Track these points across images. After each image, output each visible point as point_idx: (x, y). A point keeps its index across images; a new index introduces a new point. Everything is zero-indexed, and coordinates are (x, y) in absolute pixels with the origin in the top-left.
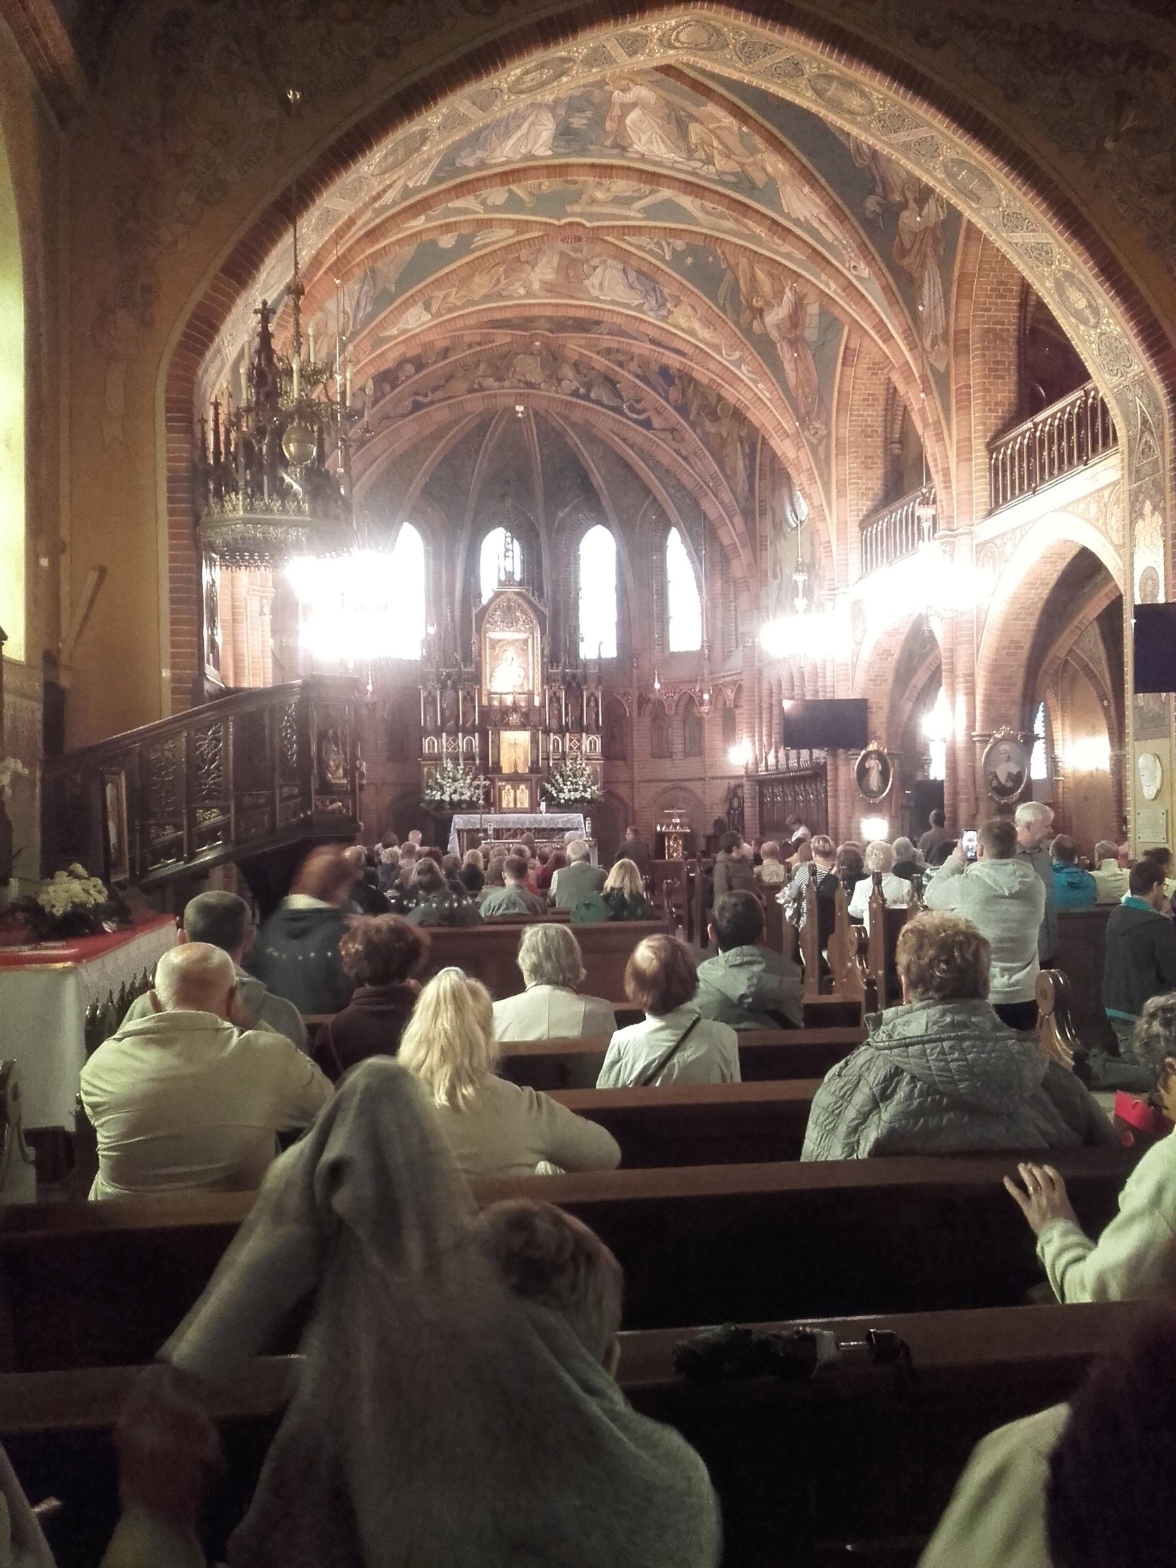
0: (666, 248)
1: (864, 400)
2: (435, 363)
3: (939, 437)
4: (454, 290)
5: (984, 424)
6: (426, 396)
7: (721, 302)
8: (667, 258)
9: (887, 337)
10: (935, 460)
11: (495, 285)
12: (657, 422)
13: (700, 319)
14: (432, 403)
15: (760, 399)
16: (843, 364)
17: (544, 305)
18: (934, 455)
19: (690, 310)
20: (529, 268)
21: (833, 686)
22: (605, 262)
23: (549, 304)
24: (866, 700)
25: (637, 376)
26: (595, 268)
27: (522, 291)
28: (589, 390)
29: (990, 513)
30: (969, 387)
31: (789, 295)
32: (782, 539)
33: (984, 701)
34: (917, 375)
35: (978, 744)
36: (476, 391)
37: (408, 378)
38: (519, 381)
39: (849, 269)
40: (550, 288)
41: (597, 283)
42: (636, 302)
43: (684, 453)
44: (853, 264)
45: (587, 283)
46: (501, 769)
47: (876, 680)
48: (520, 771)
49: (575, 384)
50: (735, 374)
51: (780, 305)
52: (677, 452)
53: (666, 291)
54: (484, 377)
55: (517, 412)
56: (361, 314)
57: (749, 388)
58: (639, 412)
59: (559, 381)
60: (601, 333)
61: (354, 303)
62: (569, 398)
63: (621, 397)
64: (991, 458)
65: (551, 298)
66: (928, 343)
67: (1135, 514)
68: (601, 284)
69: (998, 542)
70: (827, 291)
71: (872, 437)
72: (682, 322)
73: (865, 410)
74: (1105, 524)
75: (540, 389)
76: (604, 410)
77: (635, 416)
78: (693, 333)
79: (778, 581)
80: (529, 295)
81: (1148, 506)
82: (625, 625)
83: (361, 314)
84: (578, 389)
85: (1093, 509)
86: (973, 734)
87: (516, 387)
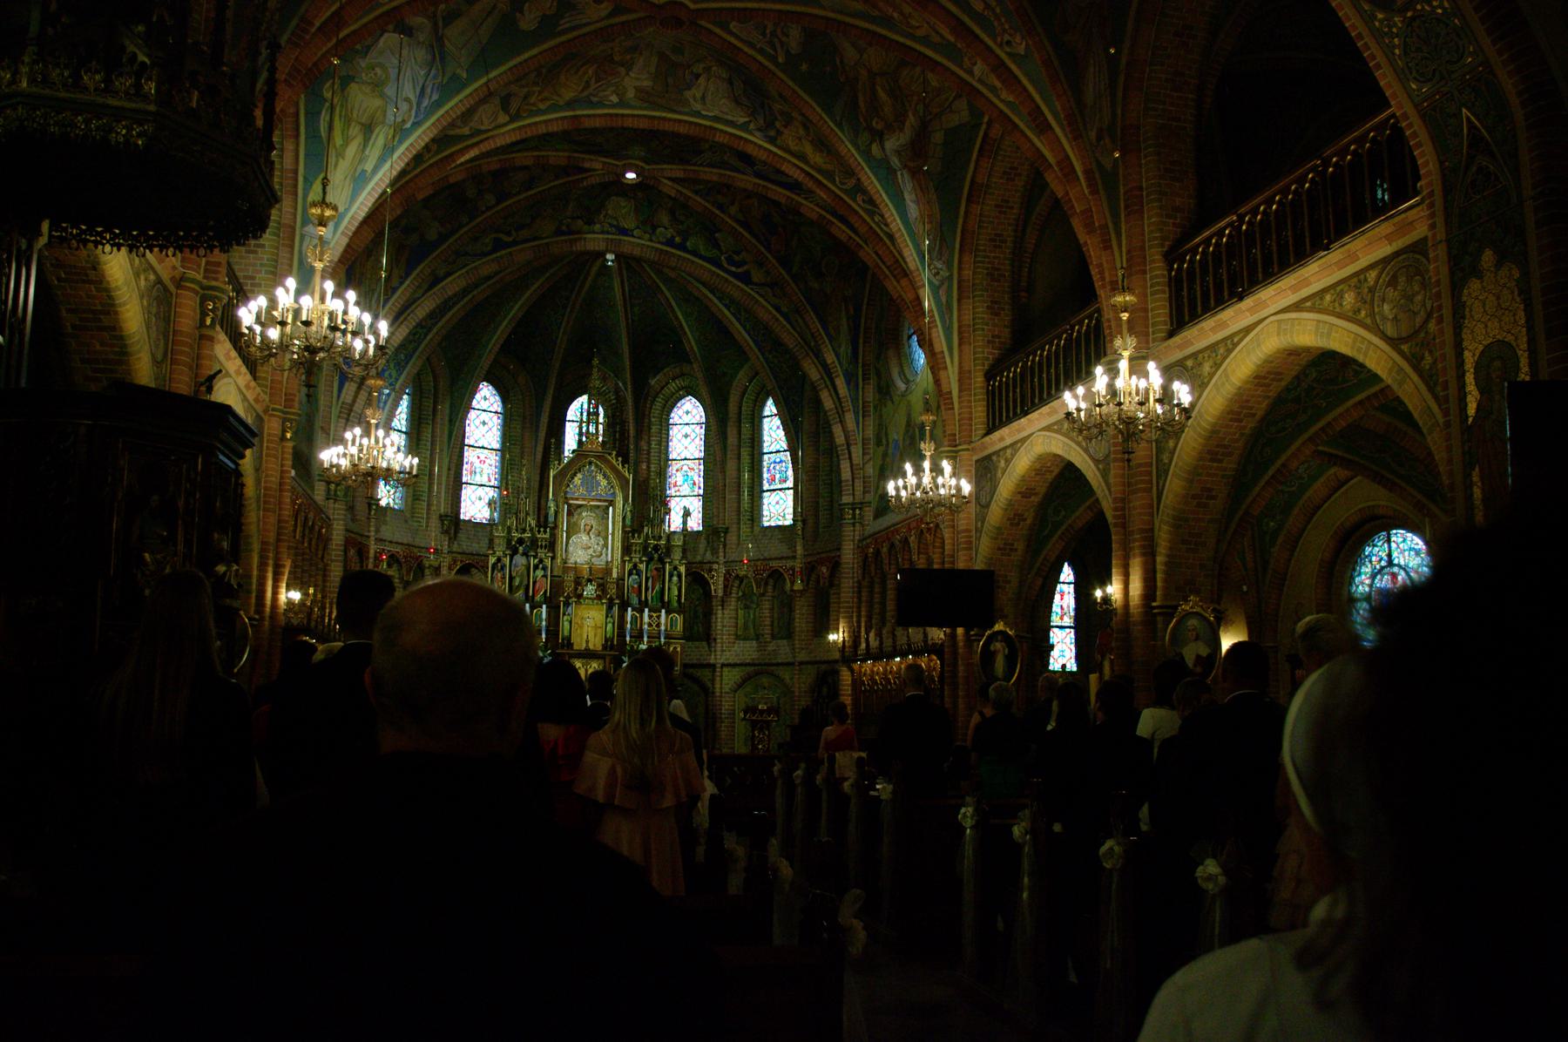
0: (779, 50)
1: (991, 240)
2: (519, 193)
3: (1107, 246)
4: (537, 89)
5: (1161, 230)
6: (509, 234)
7: (838, 119)
8: (780, 60)
9: (1043, 128)
10: (1101, 273)
11: (583, 91)
12: (757, 276)
13: (811, 142)
14: (515, 243)
15: (875, 232)
16: (969, 201)
17: (639, 116)
18: (1100, 265)
19: (802, 132)
20: (622, 70)
21: (953, 556)
22: (710, 68)
23: (645, 116)
24: (993, 572)
25: (737, 221)
26: (698, 76)
27: (615, 99)
28: (685, 240)
29: (1171, 334)
30: (1141, 188)
31: (911, 119)
32: (889, 403)
33: (1166, 564)
34: (1080, 174)
35: (1159, 619)
36: (563, 233)
37: (489, 208)
38: (611, 225)
39: (1001, 46)
40: (645, 97)
41: (698, 95)
42: (742, 120)
43: (785, 309)
44: (1007, 37)
45: (688, 94)
46: (572, 644)
47: (1005, 548)
48: (591, 647)
49: (670, 233)
50: (850, 206)
51: (901, 130)
52: (778, 309)
53: (777, 107)
54: (573, 218)
55: (608, 261)
56: (426, 103)
57: (864, 221)
58: (738, 265)
59: (654, 228)
60: (701, 165)
61: (418, 91)
62: (665, 248)
63: (719, 248)
64: (1171, 269)
65: (645, 109)
66: (1093, 135)
67: (1463, 269)
68: (703, 98)
69: (1189, 363)
70: (970, 79)
71: (999, 281)
72: (792, 144)
73: (991, 252)
74: (1372, 314)
75: (633, 236)
76: (700, 262)
77: (733, 269)
78: (802, 157)
79: (882, 449)
80: (622, 103)
81: (1488, 257)
82: (712, 496)
83: (426, 103)
84: (673, 237)
85: (1349, 298)
86: (1154, 604)
87: (608, 233)
